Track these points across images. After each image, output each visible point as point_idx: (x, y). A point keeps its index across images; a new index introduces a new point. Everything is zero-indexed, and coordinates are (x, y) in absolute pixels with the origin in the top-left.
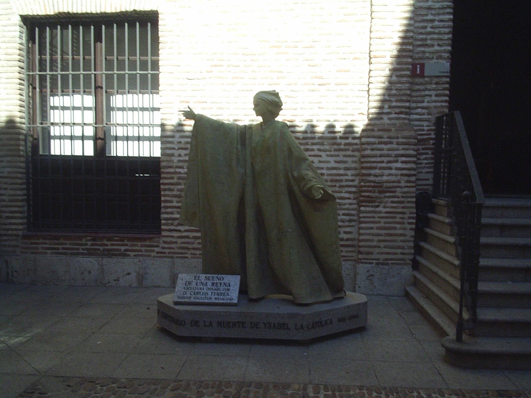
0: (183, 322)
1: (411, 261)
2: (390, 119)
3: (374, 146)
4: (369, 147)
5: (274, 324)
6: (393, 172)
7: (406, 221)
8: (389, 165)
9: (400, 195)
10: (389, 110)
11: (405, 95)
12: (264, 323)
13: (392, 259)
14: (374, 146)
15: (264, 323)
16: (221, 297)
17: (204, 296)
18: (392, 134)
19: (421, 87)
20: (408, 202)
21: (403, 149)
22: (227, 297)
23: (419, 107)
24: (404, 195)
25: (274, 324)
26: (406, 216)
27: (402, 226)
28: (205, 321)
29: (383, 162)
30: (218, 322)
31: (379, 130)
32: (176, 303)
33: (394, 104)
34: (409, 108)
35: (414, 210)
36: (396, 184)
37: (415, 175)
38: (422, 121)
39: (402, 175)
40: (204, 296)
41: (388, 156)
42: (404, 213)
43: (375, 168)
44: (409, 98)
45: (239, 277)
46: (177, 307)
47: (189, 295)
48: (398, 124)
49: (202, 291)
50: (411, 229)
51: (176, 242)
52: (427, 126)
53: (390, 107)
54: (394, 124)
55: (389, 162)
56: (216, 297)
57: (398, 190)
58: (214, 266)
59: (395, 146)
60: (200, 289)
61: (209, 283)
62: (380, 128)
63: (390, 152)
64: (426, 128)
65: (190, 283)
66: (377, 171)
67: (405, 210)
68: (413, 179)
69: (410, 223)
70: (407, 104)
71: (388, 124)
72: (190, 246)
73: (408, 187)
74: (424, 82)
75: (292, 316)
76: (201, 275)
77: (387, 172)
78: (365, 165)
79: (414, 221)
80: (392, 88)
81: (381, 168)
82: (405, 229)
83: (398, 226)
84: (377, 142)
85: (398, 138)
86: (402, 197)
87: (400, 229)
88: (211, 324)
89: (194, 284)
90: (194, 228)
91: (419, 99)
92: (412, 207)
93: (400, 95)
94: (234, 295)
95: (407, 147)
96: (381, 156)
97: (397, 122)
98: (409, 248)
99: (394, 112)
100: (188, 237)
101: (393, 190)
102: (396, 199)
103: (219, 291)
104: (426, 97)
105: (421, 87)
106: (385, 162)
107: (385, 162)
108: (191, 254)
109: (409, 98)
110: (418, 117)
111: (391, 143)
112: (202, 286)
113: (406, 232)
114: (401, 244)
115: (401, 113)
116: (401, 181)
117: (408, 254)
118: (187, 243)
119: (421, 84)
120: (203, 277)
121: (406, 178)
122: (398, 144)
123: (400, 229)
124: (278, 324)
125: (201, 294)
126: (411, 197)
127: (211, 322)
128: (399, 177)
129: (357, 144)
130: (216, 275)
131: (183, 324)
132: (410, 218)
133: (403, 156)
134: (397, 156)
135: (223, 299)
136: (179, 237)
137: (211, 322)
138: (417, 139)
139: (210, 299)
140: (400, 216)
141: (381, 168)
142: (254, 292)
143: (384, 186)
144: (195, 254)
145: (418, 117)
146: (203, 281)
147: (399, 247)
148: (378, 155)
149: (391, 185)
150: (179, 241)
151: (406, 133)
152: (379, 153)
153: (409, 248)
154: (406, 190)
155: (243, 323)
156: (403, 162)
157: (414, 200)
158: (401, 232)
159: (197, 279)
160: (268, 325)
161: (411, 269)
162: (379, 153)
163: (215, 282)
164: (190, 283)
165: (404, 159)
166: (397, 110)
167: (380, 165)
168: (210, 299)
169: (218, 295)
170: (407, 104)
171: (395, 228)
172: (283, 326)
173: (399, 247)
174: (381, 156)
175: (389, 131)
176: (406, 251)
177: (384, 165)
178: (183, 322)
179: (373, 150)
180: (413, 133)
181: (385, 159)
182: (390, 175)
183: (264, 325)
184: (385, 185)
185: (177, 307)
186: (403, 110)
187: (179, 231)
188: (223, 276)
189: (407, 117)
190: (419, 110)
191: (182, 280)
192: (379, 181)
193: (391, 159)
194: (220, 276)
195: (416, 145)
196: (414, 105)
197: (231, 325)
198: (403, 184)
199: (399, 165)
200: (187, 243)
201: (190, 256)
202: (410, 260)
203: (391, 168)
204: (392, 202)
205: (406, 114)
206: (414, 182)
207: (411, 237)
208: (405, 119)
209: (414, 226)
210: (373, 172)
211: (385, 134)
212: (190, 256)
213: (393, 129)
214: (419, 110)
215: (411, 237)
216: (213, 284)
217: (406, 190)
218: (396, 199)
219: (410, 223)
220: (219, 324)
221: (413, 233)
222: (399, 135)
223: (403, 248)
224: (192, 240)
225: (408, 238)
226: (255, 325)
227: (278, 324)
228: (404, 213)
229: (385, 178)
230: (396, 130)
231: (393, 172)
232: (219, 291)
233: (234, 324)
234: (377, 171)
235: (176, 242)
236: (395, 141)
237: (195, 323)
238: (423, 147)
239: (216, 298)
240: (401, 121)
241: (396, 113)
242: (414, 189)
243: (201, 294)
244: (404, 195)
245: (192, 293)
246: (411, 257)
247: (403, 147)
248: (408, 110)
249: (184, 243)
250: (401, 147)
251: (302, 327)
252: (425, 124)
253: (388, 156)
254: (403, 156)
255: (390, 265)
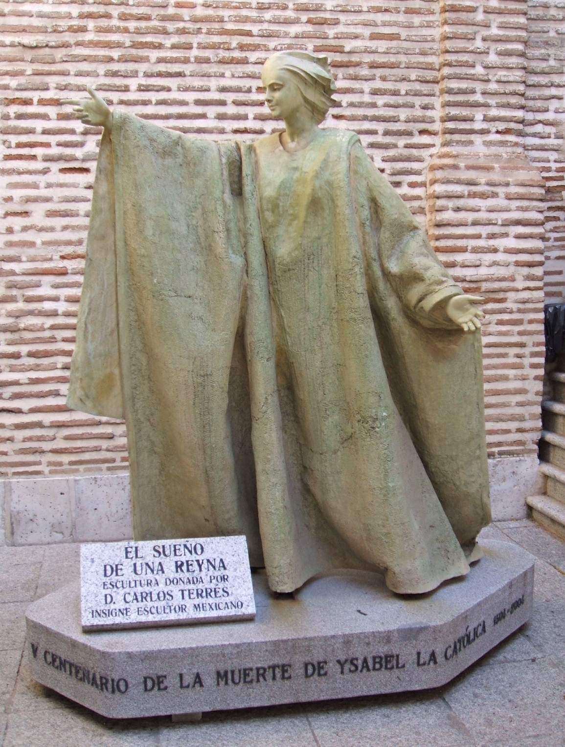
0: (122, 684)
1: (537, 444)
2: (488, 144)
3: (461, 203)
4: (451, 204)
5: (365, 661)
6: (500, 257)
7: (527, 361)
8: (492, 242)
9: (515, 307)
10: (485, 126)
11: (514, 93)
12: (339, 662)
13: (499, 444)
14: (461, 203)
15: (339, 662)
16: (211, 600)
17: (163, 603)
18: (495, 177)
19: (543, 80)
20: (531, 322)
21: (519, 209)
22: (228, 599)
23: (540, 122)
24: (521, 306)
25: (365, 661)
26: (526, 351)
27: (519, 372)
28: (181, 676)
29: (479, 237)
30: (218, 673)
31: (468, 168)
32: (90, 630)
33: (494, 112)
34: (522, 122)
35: (542, 338)
36: (504, 285)
37: (541, 264)
38: (546, 150)
39: (518, 264)
40: (163, 603)
41: (489, 223)
42: (522, 345)
43: (463, 250)
44: (523, 102)
45: (242, 539)
46: (99, 642)
47: (121, 605)
48: (505, 155)
49: (155, 590)
50: (536, 378)
51: (10, 439)
52: (555, 161)
53: (486, 119)
54: (498, 157)
55: (492, 236)
56: (197, 601)
57: (511, 295)
58: (168, 513)
59: (501, 202)
60: (149, 583)
61: (169, 564)
62: (471, 162)
63: (493, 216)
64: (554, 166)
65: (116, 570)
66: (468, 257)
67: (524, 339)
68: (538, 271)
69: (534, 366)
70: (520, 114)
71: (486, 156)
72: (46, 446)
73: (528, 289)
74: (547, 70)
75: (410, 634)
76: (140, 543)
77: (488, 258)
78: (442, 243)
79: (542, 360)
80: (490, 77)
81: (475, 250)
82: (524, 379)
83: (511, 373)
84: (466, 193)
85: (507, 185)
86: (519, 311)
87: (516, 378)
88: (198, 680)
89: (127, 572)
90: (90, 416)
91: (539, 104)
92: (537, 333)
93: (505, 93)
94: (242, 592)
95: (525, 203)
96: (475, 223)
97: (501, 150)
98: (533, 417)
99: (494, 130)
100: (39, 425)
101: (501, 295)
102: (506, 317)
103: (200, 586)
104: (553, 101)
105: (543, 80)
106: (484, 236)
107: (484, 236)
108: (50, 464)
109: (523, 102)
110: (537, 141)
111: (495, 195)
112: (150, 576)
113: (527, 385)
114: (518, 410)
115: (507, 131)
116: (516, 276)
117: (532, 430)
118: (40, 439)
119: (543, 73)
120: (147, 547)
121: (526, 271)
122: (509, 198)
123: (516, 378)
124: (374, 658)
125: (155, 597)
126: (536, 310)
127: (198, 676)
128: (512, 269)
129: (418, 198)
130: (182, 541)
131: (123, 688)
132: (534, 355)
133: (518, 223)
134: (507, 223)
135: (218, 607)
136: (19, 427)
137: (198, 676)
138: (543, 187)
139: (182, 609)
140: (516, 350)
141: (475, 250)
142: (285, 575)
143: (483, 289)
144: (60, 464)
145: (537, 141)
146: (150, 559)
147: (513, 418)
148: (470, 222)
149: (497, 285)
150: (20, 435)
151: (523, 175)
152: (470, 217)
153: (533, 417)
154: (526, 295)
155: (284, 668)
156: (518, 237)
157: (542, 316)
158: (518, 385)
159: (133, 554)
160: (347, 667)
161: (538, 461)
162: (470, 217)
163: (184, 559)
164: (116, 570)
165: (521, 230)
166: (501, 126)
167: (472, 243)
168: (182, 609)
169: (199, 595)
170: (520, 114)
171: (506, 378)
172: (387, 662)
173: (513, 418)
174: (475, 223)
175: (488, 169)
176: (527, 425)
177: (481, 243)
178: (122, 684)
179: (458, 209)
180: (536, 176)
181: (484, 231)
182: (495, 264)
183: (338, 666)
184: (485, 286)
185: (99, 642)
186: (512, 125)
187: (19, 411)
188: (201, 540)
189: (520, 140)
190: (539, 128)
191: (93, 561)
192: (474, 278)
193: (496, 230)
194: (192, 542)
195: (541, 200)
196: (530, 116)
197: (253, 674)
198: (520, 284)
199: (511, 243)
200: (40, 439)
201: (46, 470)
202: (534, 442)
203: (495, 251)
204: (500, 323)
205: (520, 134)
206: (540, 279)
207: (537, 394)
208: (516, 144)
209: (541, 372)
210: (459, 258)
211: (482, 177)
212: (46, 470)
213: (496, 166)
214: (539, 128)
215: (537, 394)
216: (179, 566)
217: (526, 295)
218: (506, 317)
219: (534, 366)
220: (222, 676)
221: (539, 386)
222: (510, 179)
223: (521, 419)
224: (51, 432)
225: (531, 397)
226: (318, 669)
227: (374, 658)
228: (522, 345)
229: (483, 272)
230: (503, 168)
231: (500, 257)
232: (200, 586)
233: (261, 673)
234: (468, 257)
235: (10, 439)
236: (501, 190)
237: (157, 683)
238: (550, 204)
239: (196, 607)
240: (509, 150)
241: (498, 132)
242: (540, 294)
243: (155, 597)
244: (521, 306)
245: (129, 598)
246: (536, 436)
247: (518, 203)
248: (521, 126)
249: (30, 439)
250: (515, 204)
251: (433, 657)
252: (553, 156)
253: (489, 223)
254: (518, 223)
255: (497, 456)
